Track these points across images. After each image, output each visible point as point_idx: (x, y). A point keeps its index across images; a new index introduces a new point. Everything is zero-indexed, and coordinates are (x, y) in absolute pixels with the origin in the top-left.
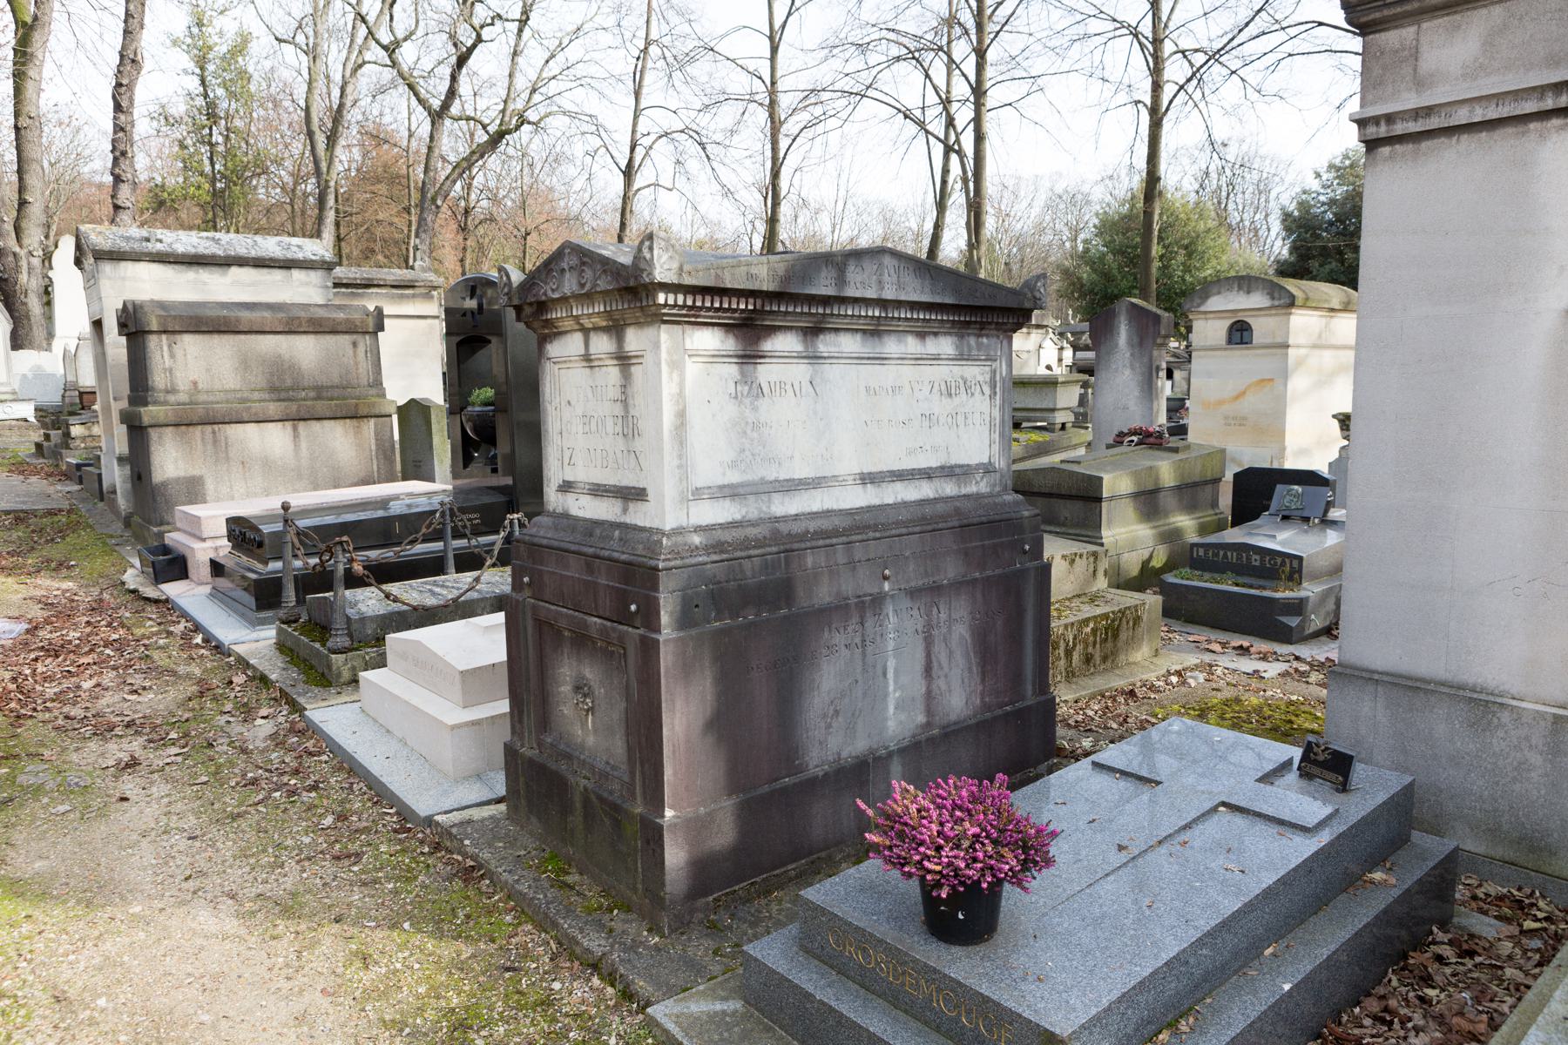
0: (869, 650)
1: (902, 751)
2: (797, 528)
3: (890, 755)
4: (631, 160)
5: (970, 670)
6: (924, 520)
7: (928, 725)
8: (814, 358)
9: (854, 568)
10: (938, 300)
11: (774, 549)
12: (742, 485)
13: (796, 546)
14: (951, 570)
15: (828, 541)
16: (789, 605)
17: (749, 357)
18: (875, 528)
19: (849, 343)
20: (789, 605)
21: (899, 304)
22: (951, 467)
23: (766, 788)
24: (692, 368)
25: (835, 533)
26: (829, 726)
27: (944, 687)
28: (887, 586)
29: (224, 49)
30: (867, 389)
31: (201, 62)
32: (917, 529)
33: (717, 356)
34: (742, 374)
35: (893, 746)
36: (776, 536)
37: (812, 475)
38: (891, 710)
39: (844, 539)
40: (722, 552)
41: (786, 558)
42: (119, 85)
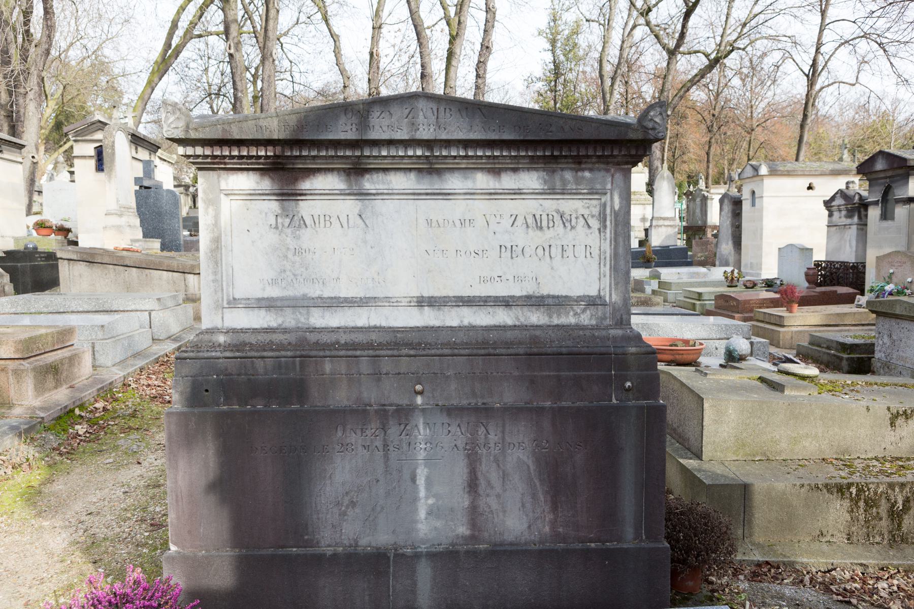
0: (393, 455)
1: (432, 556)
2: (326, 338)
3: (417, 556)
4: (815, 62)
5: (534, 496)
6: (485, 344)
7: (473, 538)
8: (362, 195)
9: (379, 380)
10: (506, 136)
11: (289, 353)
12: (282, 299)
13: (313, 353)
14: (509, 395)
15: (350, 353)
16: (302, 403)
17: (288, 195)
18: (409, 345)
19: (400, 181)
20: (302, 403)
21: (448, 143)
22: (543, 297)
23: (270, 551)
24: (226, 204)
25: (370, 346)
26: (344, 514)
27: (494, 505)
28: (419, 400)
29: (566, 32)
30: (429, 222)
31: (553, 42)
32: (467, 351)
33: (253, 195)
34: (283, 209)
35: (423, 548)
36: (302, 343)
37: (362, 295)
38: (422, 514)
39: (371, 352)
40: (238, 351)
41: (301, 363)
42: (479, 62)
